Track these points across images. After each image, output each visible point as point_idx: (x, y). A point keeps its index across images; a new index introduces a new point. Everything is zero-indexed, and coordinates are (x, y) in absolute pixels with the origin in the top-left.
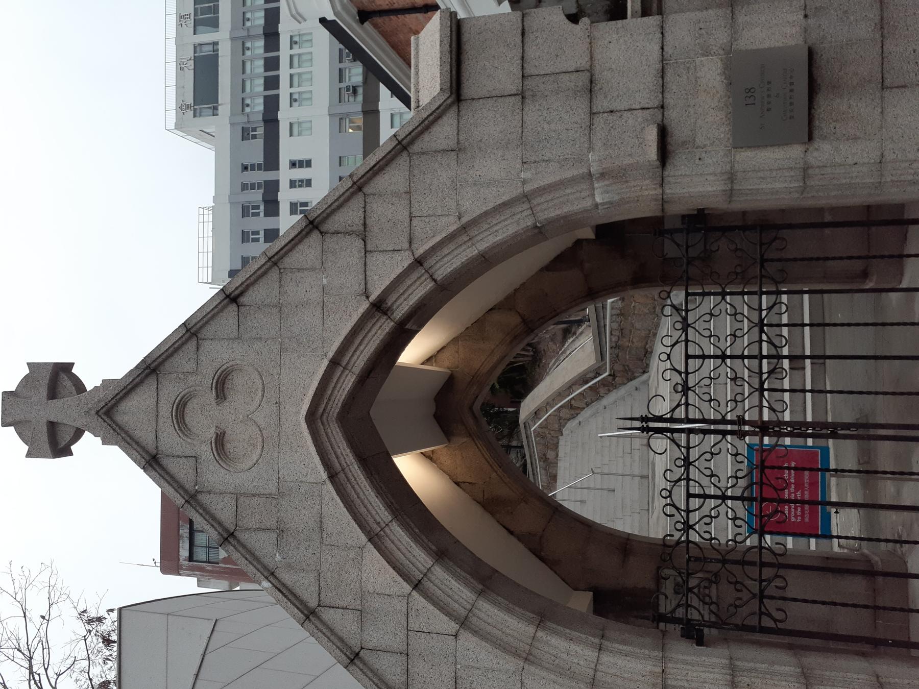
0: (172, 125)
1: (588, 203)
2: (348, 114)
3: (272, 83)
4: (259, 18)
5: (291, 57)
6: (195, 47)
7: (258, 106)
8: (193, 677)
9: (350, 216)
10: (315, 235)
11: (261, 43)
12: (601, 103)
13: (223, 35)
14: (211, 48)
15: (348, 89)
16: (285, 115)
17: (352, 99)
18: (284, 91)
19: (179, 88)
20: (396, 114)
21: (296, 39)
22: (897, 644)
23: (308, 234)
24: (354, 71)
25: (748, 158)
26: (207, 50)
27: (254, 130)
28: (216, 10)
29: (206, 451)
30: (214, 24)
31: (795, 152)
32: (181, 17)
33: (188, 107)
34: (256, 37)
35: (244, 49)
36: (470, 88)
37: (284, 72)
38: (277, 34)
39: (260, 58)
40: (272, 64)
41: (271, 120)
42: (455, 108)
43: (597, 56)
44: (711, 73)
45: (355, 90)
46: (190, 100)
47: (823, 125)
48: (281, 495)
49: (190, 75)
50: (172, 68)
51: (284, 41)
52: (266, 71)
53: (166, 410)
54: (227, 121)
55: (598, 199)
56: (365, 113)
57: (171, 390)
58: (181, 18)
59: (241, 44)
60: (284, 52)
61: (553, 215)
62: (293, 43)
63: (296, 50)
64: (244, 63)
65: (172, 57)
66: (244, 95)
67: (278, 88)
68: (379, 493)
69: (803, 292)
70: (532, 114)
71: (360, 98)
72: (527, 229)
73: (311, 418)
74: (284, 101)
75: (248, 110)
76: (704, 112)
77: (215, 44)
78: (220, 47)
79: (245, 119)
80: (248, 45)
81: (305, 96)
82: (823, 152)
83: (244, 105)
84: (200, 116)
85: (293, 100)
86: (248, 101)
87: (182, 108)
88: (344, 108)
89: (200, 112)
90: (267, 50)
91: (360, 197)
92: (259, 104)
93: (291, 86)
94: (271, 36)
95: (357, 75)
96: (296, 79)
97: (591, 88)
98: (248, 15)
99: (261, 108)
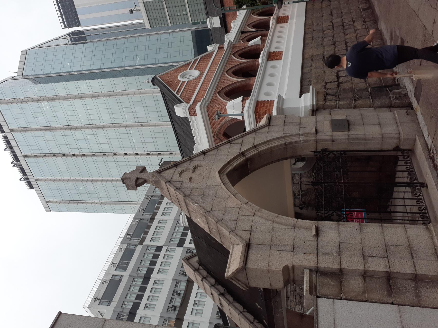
0: (86, 306)
1: (299, 140)
2: (169, 318)
3: (140, 297)
4: (144, 270)
5: (152, 288)
6: (113, 276)
7: (129, 306)
10: (229, 144)
11: (141, 280)
12: (302, 126)
13: (126, 274)
14: (119, 277)
15: (172, 307)
17: (173, 312)
18: (143, 302)
19: (98, 290)
20: (191, 323)
21: (157, 282)
22: (390, 220)
23: (227, 143)
24: (177, 300)
25: (334, 133)
26: (117, 278)
27: (123, 316)
28: (128, 264)
30: (125, 269)
31: (346, 133)
32: (112, 263)
33: (98, 299)
34: (141, 277)
35: (133, 280)
36: (271, 124)
37: (146, 294)
38: (149, 278)
39: (138, 286)
40: (143, 289)
42: (268, 127)
43: (301, 120)
45: (175, 308)
46: (100, 297)
48: (206, 188)
49: (105, 286)
50: (99, 282)
51: (151, 281)
52: (139, 292)
54: (113, 309)
55: (301, 139)
56: (177, 319)
57: (179, 169)
58: (113, 264)
59: (133, 278)
60: (150, 285)
61: (290, 141)
62: (155, 283)
63: (155, 286)
64: (131, 286)
65: (101, 277)
66: (125, 300)
67: (147, 284)
69: (362, 211)
70: (286, 127)
71: (176, 312)
72: (283, 144)
75: (124, 306)
77: (122, 276)
78: (123, 278)
79: (121, 310)
80: (136, 280)
81: (152, 306)
82: (351, 133)
83: (123, 304)
84: (102, 304)
85: (146, 306)
86: (126, 303)
87: (96, 299)
89: (103, 303)
90: (143, 283)
91: (242, 138)
92: (130, 305)
93: (147, 300)
94: (147, 278)
95: (183, 286)
96: (153, 290)
97: (300, 124)
98: (140, 269)
99: (130, 307)
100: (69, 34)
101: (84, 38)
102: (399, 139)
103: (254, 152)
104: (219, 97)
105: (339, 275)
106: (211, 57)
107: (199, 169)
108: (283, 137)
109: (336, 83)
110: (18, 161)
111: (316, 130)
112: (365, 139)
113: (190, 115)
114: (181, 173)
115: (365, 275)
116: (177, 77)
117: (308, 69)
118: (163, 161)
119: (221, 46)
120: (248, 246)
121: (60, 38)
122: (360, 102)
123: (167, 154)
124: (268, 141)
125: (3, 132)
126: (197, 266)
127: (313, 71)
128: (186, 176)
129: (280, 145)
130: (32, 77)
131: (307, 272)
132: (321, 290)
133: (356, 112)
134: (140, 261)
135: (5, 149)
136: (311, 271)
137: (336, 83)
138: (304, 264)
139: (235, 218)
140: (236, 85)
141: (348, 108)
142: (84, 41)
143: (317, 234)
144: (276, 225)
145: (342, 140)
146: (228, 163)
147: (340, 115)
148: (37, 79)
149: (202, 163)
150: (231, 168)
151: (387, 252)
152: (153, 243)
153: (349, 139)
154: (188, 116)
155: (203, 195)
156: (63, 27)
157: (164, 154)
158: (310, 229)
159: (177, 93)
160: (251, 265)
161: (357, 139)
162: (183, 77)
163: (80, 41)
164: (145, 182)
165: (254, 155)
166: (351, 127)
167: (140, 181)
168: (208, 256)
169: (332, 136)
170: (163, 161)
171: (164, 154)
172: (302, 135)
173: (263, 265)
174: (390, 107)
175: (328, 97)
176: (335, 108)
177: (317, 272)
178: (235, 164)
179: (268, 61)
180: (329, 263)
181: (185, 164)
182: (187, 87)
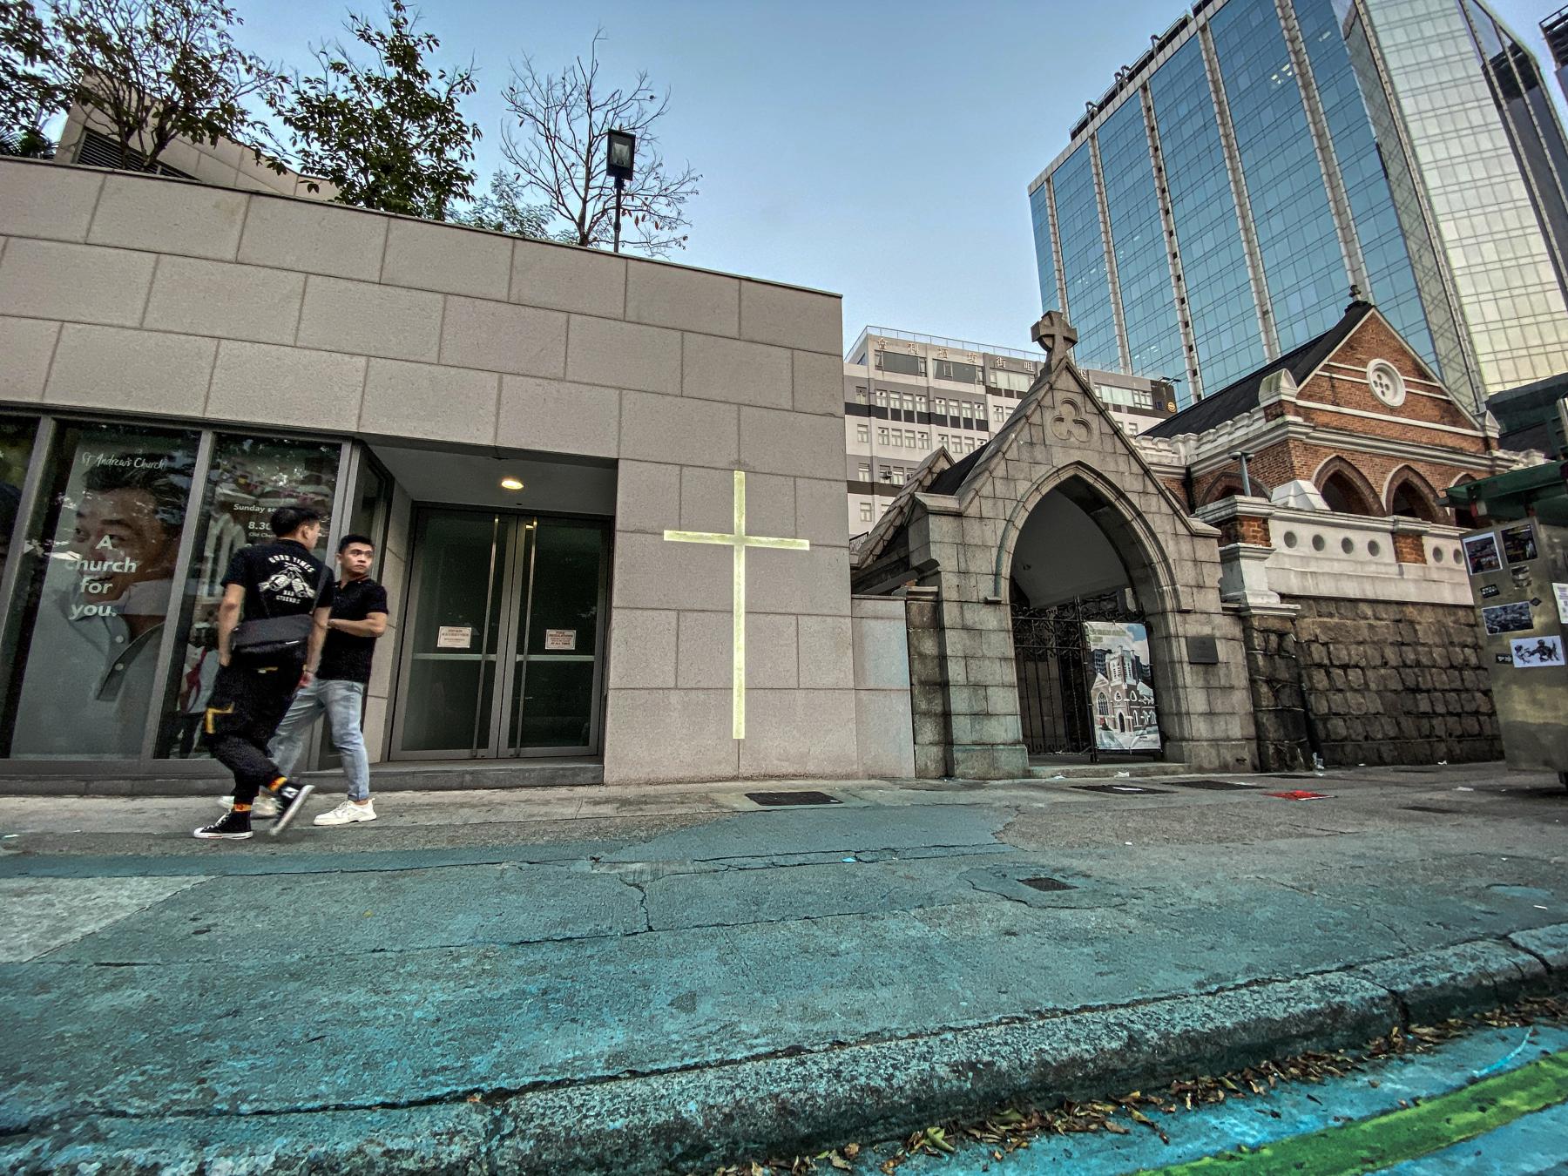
8: (276, 264)
9: (1151, 489)
16: (875, 422)
18: (889, 423)
29: (1057, 413)
30: (939, 375)
31: (1186, 659)
36: (1197, 540)
40: (909, 416)
41: (870, 411)
44: (1207, 630)
46: (887, 349)
47: (1195, 668)
51: (924, 428)
53: (1070, 395)
57: (1079, 399)
59: (927, 394)
68: (49, 461)
70: (1190, 564)
73: (1079, 463)
74: (883, 423)
76: (1195, 627)
82: (1187, 668)
85: (883, 429)
88: (876, 468)
97: (1199, 587)
100: (1516, 48)
101: (1511, 91)
102: (1183, 739)
103: (1128, 514)
104: (1390, 475)
105: (938, 626)
106: (1454, 424)
107: (1083, 431)
108: (1165, 559)
109: (1326, 661)
110: (1131, 77)
111: (1188, 612)
112: (1176, 687)
113: (1265, 408)
114: (1072, 403)
115: (942, 658)
116: (1377, 356)
117: (1370, 613)
118: (1175, 385)
119: (1494, 444)
120: (958, 515)
121: (1498, 29)
122: (1264, 689)
123: (1195, 389)
124: (1153, 535)
125: (1197, 11)
126: (937, 470)
127: (1362, 622)
128: (1066, 411)
129: (1148, 555)
130: (1362, 11)
131: (935, 589)
132: (914, 606)
133: (1240, 678)
134: (959, 398)
135: (1155, 37)
136: (937, 594)
137: (1326, 661)
138: (944, 585)
139: (998, 494)
140: (1367, 492)
141: (1250, 669)
142: (1501, 96)
143: (987, 602)
144: (994, 551)
145: (1170, 651)
146: (1099, 475)
147: (1230, 653)
148: (1357, 27)
149: (1096, 432)
150: (1091, 481)
151: (978, 687)
152: (991, 410)
153: (1172, 662)
154: (1263, 405)
155: (1032, 444)
156: (1547, 23)
157: (1195, 383)
158: (996, 592)
159: (1327, 368)
160: (932, 519)
161: (1174, 675)
162: (1380, 369)
163: (1501, 86)
164: (1049, 350)
165: (1122, 515)
166: (1201, 668)
167: (1048, 342)
168: (951, 478)
169: (1177, 636)
170: (1175, 385)
171: (1195, 383)
172: (1175, 590)
173: (934, 536)
174: (1260, 738)
175: (1273, 637)
176: (1248, 648)
177: (938, 601)
178: (1099, 486)
179: (1393, 533)
180: (950, 614)
181: (1090, 406)
182: (1348, 385)
